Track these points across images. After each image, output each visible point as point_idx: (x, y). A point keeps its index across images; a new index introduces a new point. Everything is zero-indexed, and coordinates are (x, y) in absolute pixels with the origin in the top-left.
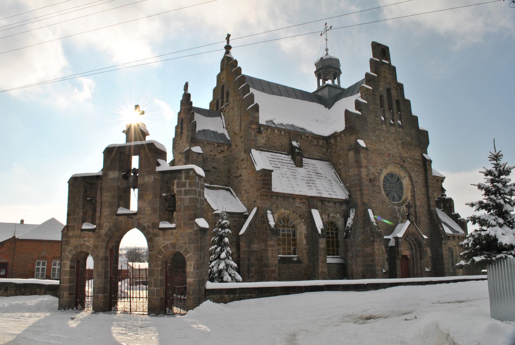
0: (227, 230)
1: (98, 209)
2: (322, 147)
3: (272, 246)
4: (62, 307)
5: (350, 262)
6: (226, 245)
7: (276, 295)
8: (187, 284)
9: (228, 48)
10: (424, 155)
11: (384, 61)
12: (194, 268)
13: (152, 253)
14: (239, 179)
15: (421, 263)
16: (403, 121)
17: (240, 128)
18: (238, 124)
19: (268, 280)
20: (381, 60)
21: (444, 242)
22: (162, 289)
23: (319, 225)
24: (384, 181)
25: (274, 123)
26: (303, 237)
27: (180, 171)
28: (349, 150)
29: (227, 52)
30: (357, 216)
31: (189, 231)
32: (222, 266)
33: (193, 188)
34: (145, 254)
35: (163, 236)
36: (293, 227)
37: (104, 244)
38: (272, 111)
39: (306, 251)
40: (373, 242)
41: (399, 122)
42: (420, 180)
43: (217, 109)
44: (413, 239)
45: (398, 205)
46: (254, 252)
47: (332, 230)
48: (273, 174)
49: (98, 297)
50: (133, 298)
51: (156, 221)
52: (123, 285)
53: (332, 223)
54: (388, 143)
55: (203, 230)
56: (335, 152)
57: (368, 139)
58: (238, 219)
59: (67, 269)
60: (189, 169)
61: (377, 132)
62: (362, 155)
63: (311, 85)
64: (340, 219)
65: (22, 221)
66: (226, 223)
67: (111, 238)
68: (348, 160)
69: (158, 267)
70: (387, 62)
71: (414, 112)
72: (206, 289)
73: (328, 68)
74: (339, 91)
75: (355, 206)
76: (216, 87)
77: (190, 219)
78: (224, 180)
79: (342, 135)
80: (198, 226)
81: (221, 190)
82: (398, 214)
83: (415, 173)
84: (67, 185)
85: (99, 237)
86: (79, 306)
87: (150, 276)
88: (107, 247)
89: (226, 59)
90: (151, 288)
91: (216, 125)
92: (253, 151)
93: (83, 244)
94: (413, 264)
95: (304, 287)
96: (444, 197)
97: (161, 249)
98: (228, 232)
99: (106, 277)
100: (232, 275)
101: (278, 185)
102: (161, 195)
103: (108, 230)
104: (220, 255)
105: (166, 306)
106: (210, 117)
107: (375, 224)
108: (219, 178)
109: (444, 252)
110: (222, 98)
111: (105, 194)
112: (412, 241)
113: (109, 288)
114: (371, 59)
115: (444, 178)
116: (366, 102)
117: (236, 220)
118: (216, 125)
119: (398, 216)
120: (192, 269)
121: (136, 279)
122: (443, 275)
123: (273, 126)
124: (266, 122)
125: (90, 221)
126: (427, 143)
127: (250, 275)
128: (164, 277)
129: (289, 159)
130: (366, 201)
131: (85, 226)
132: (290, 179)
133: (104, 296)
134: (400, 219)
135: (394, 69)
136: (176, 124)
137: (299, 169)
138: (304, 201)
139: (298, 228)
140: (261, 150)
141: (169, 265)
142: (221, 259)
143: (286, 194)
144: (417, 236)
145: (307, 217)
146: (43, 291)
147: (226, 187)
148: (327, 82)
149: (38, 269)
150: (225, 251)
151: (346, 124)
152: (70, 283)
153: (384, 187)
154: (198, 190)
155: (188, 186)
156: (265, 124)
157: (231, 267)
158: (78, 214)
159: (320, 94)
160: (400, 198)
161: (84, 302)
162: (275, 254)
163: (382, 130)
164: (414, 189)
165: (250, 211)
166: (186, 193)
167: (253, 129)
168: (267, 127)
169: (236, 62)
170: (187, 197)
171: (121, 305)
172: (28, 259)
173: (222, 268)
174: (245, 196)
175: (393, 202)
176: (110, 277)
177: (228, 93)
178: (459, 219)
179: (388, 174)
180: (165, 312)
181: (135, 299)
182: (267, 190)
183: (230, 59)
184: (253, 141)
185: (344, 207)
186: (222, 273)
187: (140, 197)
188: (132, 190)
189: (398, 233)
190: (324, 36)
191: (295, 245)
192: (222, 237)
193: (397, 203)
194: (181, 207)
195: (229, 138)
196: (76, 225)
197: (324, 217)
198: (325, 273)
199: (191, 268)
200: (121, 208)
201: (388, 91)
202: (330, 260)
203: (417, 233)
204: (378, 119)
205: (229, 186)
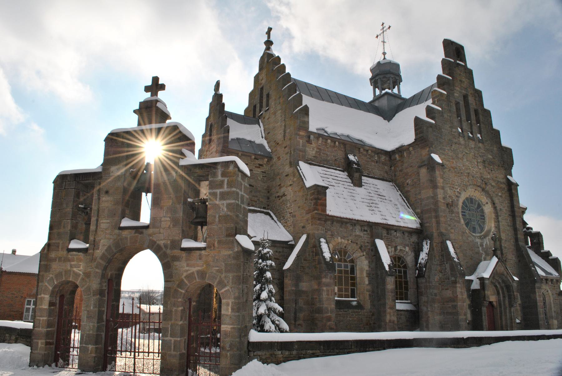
0: (269, 262)
1: (93, 219)
2: (384, 164)
3: (327, 285)
4: (34, 362)
5: (424, 309)
6: (268, 281)
7: (348, 353)
9: (269, 43)
10: (509, 177)
11: (458, 62)
12: (232, 309)
14: (281, 200)
15: (510, 312)
16: (483, 134)
17: (284, 136)
18: (282, 131)
19: (322, 331)
20: (455, 61)
21: (537, 285)
22: (182, 340)
23: (386, 260)
24: (462, 208)
25: (326, 132)
26: (365, 275)
27: (214, 165)
28: (420, 167)
29: (268, 48)
30: (433, 250)
31: (226, 252)
32: (262, 309)
33: (234, 189)
34: (159, 298)
35: (187, 260)
36: (352, 261)
37: (99, 271)
38: (322, 118)
39: (368, 293)
40: (455, 282)
41: (479, 135)
42: (504, 207)
43: (254, 116)
44: (500, 281)
45: (480, 237)
47: (399, 267)
50: (139, 352)
51: (177, 238)
52: (125, 334)
53: (399, 258)
54: (467, 161)
55: (247, 252)
56: (401, 171)
57: (443, 154)
58: (281, 250)
59: (45, 306)
60: (228, 162)
61: (453, 147)
62: (437, 173)
63: (367, 94)
64: (410, 253)
65: (14, 252)
66: (268, 252)
67: (109, 262)
68: (419, 180)
69: (178, 307)
70: (463, 64)
71: (495, 126)
72: (249, 342)
73: (386, 75)
74: (400, 101)
75: (429, 237)
76: (252, 91)
77: (228, 235)
78: (262, 202)
79: (411, 149)
80: (241, 246)
81: (258, 214)
82: (481, 248)
83: (499, 199)
85: (93, 260)
86: (61, 361)
87: (164, 320)
88: (103, 276)
89: (266, 55)
90: (166, 339)
91: (254, 133)
92: (301, 164)
93: (70, 271)
94: (501, 313)
95: (387, 340)
96: (530, 230)
97: (182, 280)
98: (271, 265)
99: (100, 320)
100: (277, 322)
101: (335, 206)
102: (185, 200)
103: (106, 250)
104: (259, 295)
105: (188, 367)
106: (245, 124)
107: (456, 260)
108: (256, 199)
109: (538, 299)
110: (261, 102)
111: (104, 199)
112: (499, 283)
113: (104, 336)
114: (443, 59)
115: (526, 209)
116: (440, 109)
117: (279, 250)
118: (254, 133)
119: (481, 252)
120: (230, 310)
122: (537, 327)
123: (325, 134)
124: (317, 129)
125: (82, 237)
126: (511, 163)
127: (297, 323)
128: (187, 322)
129: (346, 177)
130: (443, 231)
131: (74, 245)
132: (346, 201)
134: (483, 256)
135: (470, 72)
136: (204, 132)
137: (357, 189)
138: (366, 229)
139: (358, 263)
140: (310, 164)
141: (194, 304)
142: (261, 301)
143: (344, 218)
144: (506, 277)
145: (369, 249)
146: (13, 337)
147: (265, 211)
148: (383, 92)
149: (28, 309)
150: (267, 290)
151: (416, 134)
153: (463, 215)
154: (240, 193)
155: (225, 186)
156: (315, 131)
157: (275, 312)
158: (64, 227)
159: (376, 104)
160: (482, 229)
161: (69, 356)
162: (330, 295)
163: (459, 144)
164: (498, 218)
165: (296, 239)
166: (223, 196)
168: (318, 136)
169: (278, 59)
172: (17, 297)
173: (263, 312)
174: (290, 220)
175: (474, 234)
176: (107, 320)
177: (268, 96)
178: (550, 258)
179: (467, 199)
181: (141, 354)
183: (272, 55)
184: (300, 151)
185: (414, 239)
186: (263, 319)
187: (155, 203)
188: (144, 194)
189: (484, 272)
190: (380, 38)
191: (353, 285)
192: (262, 271)
193: (479, 235)
194: (215, 217)
195: (269, 150)
196: (61, 242)
197: (390, 250)
198: (394, 321)
199: (227, 310)
200: (126, 218)
201: (465, 97)
202: (400, 306)
203: (506, 274)
204: (454, 130)
205: (268, 209)
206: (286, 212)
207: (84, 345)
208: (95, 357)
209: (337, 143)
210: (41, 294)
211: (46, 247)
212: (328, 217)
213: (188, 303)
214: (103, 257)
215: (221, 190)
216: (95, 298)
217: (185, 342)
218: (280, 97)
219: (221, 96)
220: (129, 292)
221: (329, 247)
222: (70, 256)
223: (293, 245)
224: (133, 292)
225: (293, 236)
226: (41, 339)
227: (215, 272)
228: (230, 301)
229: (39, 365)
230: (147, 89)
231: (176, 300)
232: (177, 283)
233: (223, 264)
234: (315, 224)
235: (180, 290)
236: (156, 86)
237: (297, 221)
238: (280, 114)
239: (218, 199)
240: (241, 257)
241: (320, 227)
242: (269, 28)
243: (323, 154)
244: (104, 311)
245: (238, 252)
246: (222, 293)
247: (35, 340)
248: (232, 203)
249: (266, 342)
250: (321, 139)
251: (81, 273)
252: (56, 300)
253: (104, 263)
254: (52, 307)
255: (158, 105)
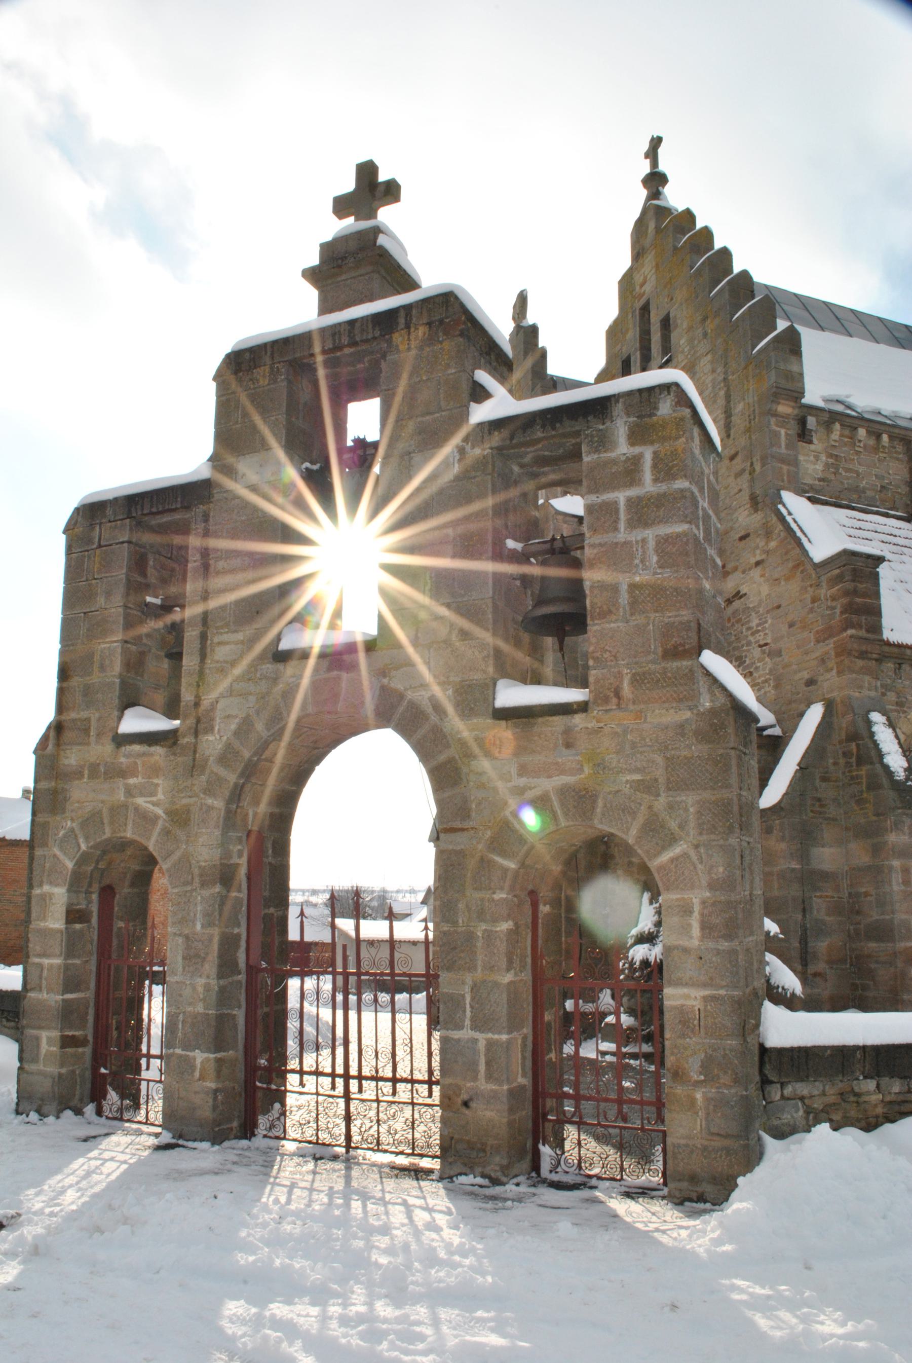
8: (669, 1018)
9: (655, 181)
12: (706, 927)
13: (460, 841)
22: (514, 1040)
25: (849, 407)
31: (667, 715)
46: (825, 876)
48: (883, 570)
49: (189, 1063)
51: (477, 676)
52: (308, 997)
69: (495, 921)
84: (61, 541)
86: (113, 1096)
89: (651, 213)
90: (456, 1035)
92: (788, 497)
93: (125, 806)
99: (226, 966)
105: (537, 1136)
120: (696, 931)
121: (375, 977)
123: (849, 412)
124: (826, 401)
127: (811, 969)
128: (527, 976)
131: (135, 722)
133: (218, 1061)
141: (545, 909)
152: (66, 990)
155: (648, 475)
156: (821, 404)
158: (102, 668)
166: (643, 512)
167: (783, 420)
170: (650, 534)
171: (304, 1102)
176: (249, 967)
177: (666, 324)
180: (536, 1166)
182: (862, 633)
184: (783, 461)
196: (94, 716)
199: (685, 929)
206: (749, 644)
207: (178, 1051)
208: (216, 1091)
209: (885, 437)
210: (41, 885)
211: (52, 734)
212: (886, 649)
213: (527, 909)
214: (227, 757)
215: (633, 492)
216: (206, 893)
217: (524, 1045)
218: (705, 319)
219: (533, 331)
220: (303, 891)
221: (897, 737)
222: (122, 760)
223: (778, 737)
224: (314, 892)
225: (775, 713)
226: (49, 1028)
227: (626, 789)
228: (696, 898)
229: (45, 1109)
230: (342, 206)
231: (486, 895)
232: (489, 833)
233: (660, 760)
234: (852, 671)
235: (499, 860)
236: (372, 190)
237: (785, 666)
238: (709, 367)
239: (622, 525)
240: (730, 730)
241: (867, 678)
242: (653, 139)
243: (848, 470)
244: (239, 935)
245: (712, 712)
246: (661, 868)
247: (34, 1032)
248: (678, 535)
249: (824, 1048)
250: (837, 426)
251: (159, 811)
252: (90, 902)
253: (232, 778)
254: (78, 926)
255: (382, 240)
